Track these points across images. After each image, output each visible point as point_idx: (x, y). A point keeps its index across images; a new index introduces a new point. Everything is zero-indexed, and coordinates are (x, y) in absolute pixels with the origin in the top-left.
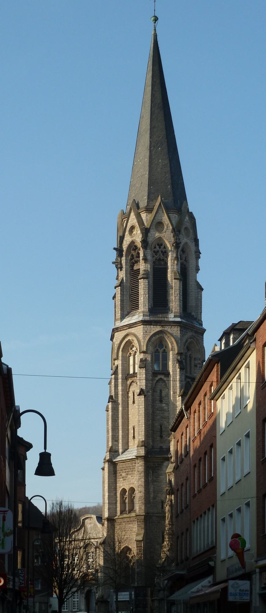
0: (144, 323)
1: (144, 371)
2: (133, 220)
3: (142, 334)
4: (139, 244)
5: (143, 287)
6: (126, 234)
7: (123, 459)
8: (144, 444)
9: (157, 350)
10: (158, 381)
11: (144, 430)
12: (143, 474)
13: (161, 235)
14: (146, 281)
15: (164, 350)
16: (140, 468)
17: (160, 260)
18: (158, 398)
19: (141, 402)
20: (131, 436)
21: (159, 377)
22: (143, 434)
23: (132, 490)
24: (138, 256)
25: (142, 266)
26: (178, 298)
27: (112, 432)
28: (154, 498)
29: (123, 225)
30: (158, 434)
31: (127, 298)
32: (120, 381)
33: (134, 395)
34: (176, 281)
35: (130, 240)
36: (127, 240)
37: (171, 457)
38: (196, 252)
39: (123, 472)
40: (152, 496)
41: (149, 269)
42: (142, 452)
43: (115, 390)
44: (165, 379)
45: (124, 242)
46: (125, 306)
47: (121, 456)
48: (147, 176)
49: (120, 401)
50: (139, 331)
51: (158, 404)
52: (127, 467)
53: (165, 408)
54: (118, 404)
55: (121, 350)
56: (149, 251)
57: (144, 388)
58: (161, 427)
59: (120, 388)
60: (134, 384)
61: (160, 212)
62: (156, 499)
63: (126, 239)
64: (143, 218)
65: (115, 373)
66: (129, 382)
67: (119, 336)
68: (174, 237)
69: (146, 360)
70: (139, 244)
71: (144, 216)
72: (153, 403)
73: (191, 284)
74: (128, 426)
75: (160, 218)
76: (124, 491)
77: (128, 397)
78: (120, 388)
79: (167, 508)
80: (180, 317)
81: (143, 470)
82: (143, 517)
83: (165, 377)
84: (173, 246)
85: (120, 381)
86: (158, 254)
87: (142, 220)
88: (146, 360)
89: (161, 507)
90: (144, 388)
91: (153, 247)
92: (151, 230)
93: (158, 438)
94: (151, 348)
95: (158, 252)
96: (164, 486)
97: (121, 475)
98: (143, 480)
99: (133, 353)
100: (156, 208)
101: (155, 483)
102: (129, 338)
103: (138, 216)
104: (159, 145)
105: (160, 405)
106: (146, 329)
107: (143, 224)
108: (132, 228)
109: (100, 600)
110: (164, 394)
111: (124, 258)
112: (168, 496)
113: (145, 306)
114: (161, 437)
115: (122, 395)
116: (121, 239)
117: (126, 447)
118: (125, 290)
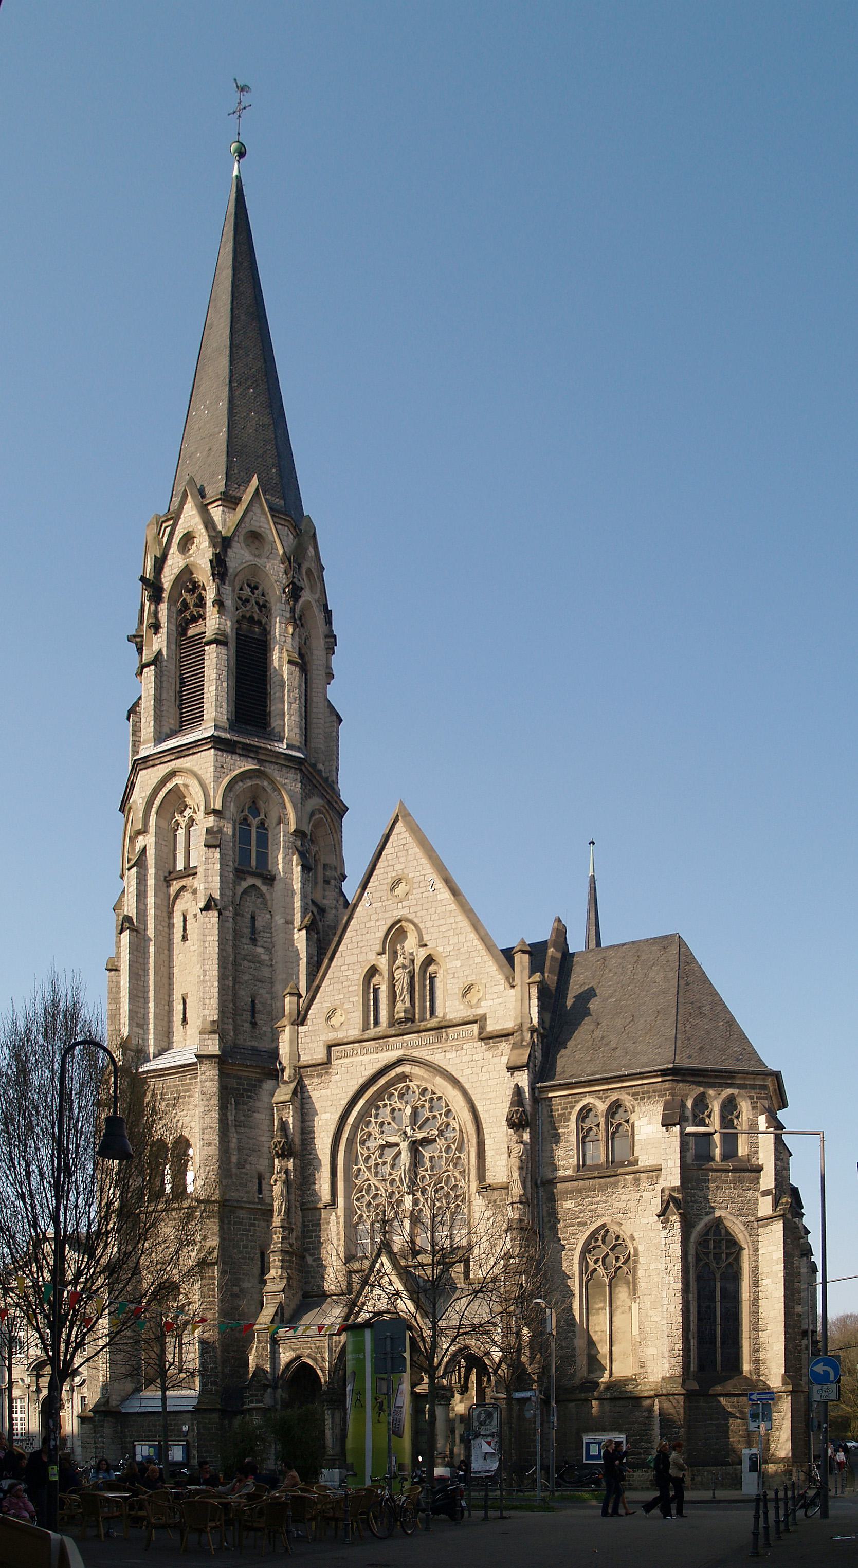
0: (217, 743)
1: (217, 855)
2: (190, 518)
3: (212, 769)
4: (204, 574)
5: (214, 666)
6: (171, 551)
7: (159, 1067)
8: (218, 1028)
9: (245, 819)
10: (245, 892)
11: (216, 995)
12: (215, 1101)
13: (260, 562)
14: (223, 650)
15: (262, 823)
16: (208, 1084)
17: (251, 620)
18: (247, 931)
19: (209, 926)
20: (177, 1017)
21: (251, 881)
22: (216, 1006)
24: (201, 602)
25: (212, 622)
26: (295, 706)
28: (240, 1165)
29: (160, 543)
30: (247, 1016)
31: (169, 695)
32: (151, 882)
33: (185, 920)
34: (293, 668)
35: (182, 564)
36: (174, 564)
37: (283, 1070)
38: (326, 637)
40: (234, 1159)
41: (229, 630)
42: (213, 1048)
44: (264, 889)
45: (166, 570)
46: (164, 713)
47: (152, 1063)
48: (223, 435)
49: (151, 933)
50: (205, 762)
51: (246, 947)
54: (147, 940)
55: (154, 810)
56: (227, 589)
57: (217, 895)
58: (253, 1001)
59: (151, 900)
60: (187, 895)
61: (256, 509)
62: (244, 1167)
63: (169, 562)
64: (215, 518)
65: (140, 862)
66: (173, 889)
67: (148, 779)
68: (286, 573)
69: (220, 831)
70: (204, 574)
71: (216, 512)
72: (235, 938)
73: (318, 709)
77: (171, 926)
78: (151, 900)
79: (277, 1189)
81: (215, 1090)
83: (264, 884)
85: (151, 882)
86: (249, 606)
87: (213, 521)
88: (220, 831)
89: (256, 1187)
90: (217, 895)
91: (238, 587)
92: (235, 544)
93: (247, 1026)
94: (232, 807)
95: (247, 601)
96: (264, 1139)
98: (215, 1114)
99: (183, 822)
100: (247, 497)
101: (242, 1130)
102: (177, 780)
103: (204, 510)
104: (249, 383)
106: (223, 760)
107: (214, 527)
108: (188, 539)
109: (103, 1408)
110: (259, 924)
111: (163, 606)
112: (276, 1161)
113: (218, 707)
114: (254, 1024)
115: (156, 916)
116: (159, 563)
117: (164, 1045)
118: (165, 678)
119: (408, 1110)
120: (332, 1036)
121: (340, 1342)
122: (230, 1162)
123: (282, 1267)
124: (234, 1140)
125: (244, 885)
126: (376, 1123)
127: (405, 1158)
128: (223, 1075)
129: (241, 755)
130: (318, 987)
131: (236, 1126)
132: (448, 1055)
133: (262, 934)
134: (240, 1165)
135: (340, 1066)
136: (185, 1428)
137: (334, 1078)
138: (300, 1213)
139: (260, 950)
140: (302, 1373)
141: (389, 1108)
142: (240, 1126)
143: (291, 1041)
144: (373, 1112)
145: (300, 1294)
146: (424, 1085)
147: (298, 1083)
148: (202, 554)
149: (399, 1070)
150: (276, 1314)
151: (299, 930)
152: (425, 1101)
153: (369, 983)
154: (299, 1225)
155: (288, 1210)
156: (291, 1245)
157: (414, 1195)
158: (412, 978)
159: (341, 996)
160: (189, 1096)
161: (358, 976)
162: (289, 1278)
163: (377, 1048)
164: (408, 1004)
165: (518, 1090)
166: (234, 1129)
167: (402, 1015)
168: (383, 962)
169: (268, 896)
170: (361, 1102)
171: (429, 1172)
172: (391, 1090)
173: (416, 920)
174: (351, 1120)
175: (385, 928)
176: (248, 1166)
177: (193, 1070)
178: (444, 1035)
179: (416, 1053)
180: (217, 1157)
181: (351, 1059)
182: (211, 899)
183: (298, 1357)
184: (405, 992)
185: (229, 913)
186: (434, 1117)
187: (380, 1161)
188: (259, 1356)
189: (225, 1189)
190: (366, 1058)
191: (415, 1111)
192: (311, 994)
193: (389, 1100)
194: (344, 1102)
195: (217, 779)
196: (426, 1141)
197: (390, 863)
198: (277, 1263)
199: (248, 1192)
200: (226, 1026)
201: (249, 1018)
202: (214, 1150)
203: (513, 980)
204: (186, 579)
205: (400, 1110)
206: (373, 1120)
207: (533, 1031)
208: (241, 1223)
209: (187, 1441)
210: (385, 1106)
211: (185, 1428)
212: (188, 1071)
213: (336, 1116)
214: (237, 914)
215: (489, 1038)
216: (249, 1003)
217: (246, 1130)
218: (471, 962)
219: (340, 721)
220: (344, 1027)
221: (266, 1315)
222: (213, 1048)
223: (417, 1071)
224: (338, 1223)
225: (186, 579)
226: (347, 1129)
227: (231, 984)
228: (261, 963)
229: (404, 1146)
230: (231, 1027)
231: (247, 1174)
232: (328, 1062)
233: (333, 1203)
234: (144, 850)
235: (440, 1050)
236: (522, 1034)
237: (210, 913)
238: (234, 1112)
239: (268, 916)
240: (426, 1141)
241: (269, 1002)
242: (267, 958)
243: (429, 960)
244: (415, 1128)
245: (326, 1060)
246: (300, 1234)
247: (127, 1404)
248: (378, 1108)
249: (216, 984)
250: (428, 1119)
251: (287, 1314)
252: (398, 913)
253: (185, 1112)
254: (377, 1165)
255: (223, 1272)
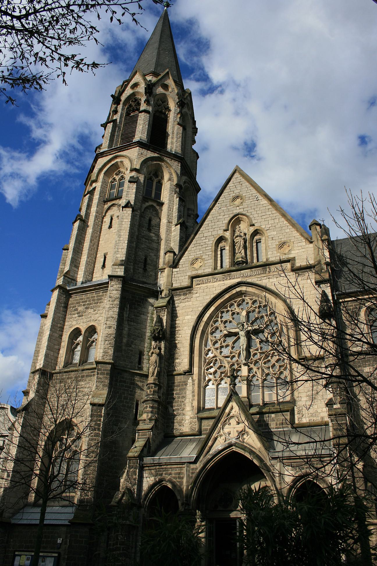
3: (137, 154)
10: (147, 208)
11: (126, 247)
12: (117, 302)
16: (114, 292)
18: (146, 225)
21: (150, 203)
23: (92, 330)
27: (73, 254)
28: (128, 345)
36: (128, 91)
39: (80, 306)
40: (125, 340)
43: (87, 209)
44: (158, 207)
48: (154, 60)
49: (91, 222)
52: (88, 298)
53: (154, 238)
57: (132, 203)
62: (131, 346)
66: (106, 206)
74: (64, 322)
75: (46, 312)
76: (77, 332)
80: (113, 360)
82: (109, 367)
84: (177, 104)
89: (137, 360)
90: (132, 203)
93: (141, 270)
97: (77, 310)
98: (117, 310)
101: (132, 323)
105: (147, 233)
110: (153, 222)
114: (145, 270)
119: (244, 313)
120: (194, 273)
121: (197, 469)
122: (122, 342)
123: (152, 412)
124: (126, 329)
125: (147, 204)
126: (222, 321)
127: (243, 341)
128: (124, 290)
129: (151, 151)
130: (187, 248)
131: (128, 320)
132: (271, 280)
133: (154, 227)
134: (128, 345)
135: (198, 289)
136: (59, 541)
137: (194, 296)
138: (166, 377)
139: (152, 235)
140: (164, 494)
141: (230, 313)
142: (131, 321)
143: (168, 276)
144: (220, 315)
145: (163, 434)
146: (255, 298)
147: (171, 298)
148: (142, 88)
149: (238, 289)
150: (145, 446)
151: (176, 225)
152: (256, 308)
153: (218, 246)
154: (166, 385)
155: (159, 373)
156: (159, 397)
157: (249, 366)
158: (245, 242)
159: (201, 252)
160: (100, 302)
161: (212, 242)
162: (156, 420)
163: (223, 278)
164: (243, 254)
165: (324, 294)
166: (126, 323)
167: (240, 259)
168: (228, 235)
169: (159, 211)
170: (212, 308)
171: (259, 351)
172: (232, 302)
173: (248, 214)
174: (205, 318)
175: (229, 219)
176: (133, 346)
177: (105, 287)
178: (268, 269)
179: (249, 280)
180: (114, 336)
181: (206, 285)
182: (129, 202)
183: (161, 481)
184: (241, 248)
185: (138, 213)
186: (262, 317)
187: (224, 344)
188: (128, 479)
189: (115, 356)
190: (216, 284)
191: (248, 313)
192: (181, 253)
193: (230, 308)
194: (201, 309)
195: (138, 158)
196: (256, 332)
197: (232, 190)
198: (148, 409)
199: (132, 362)
200: (129, 266)
201: (143, 267)
202: (113, 331)
203: (311, 239)
204: (133, 99)
205: (238, 314)
206: (219, 319)
207: (327, 264)
208: (125, 382)
209: (59, 554)
210: (228, 311)
211: (59, 541)
212: (102, 288)
213: (195, 317)
214: (141, 216)
215: (298, 270)
216: (143, 259)
217: (135, 324)
218: (283, 231)
219: (198, 157)
220: (203, 268)
221: (134, 452)
222: (120, 272)
223: (250, 289)
224: (193, 384)
225: (133, 99)
226: (202, 325)
227: (134, 245)
228: (152, 241)
229: (242, 333)
230: (132, 267)
231: (132, 351)
232: (189, 288)
233: (189, 372)
234: (95, 188)
235: (265, 278)
236: (320, 266)
237: (127, 209)
238: (128, 312)
239: (158, 220)
240: (256, 332)
241: (155, 260)
242: (156, 239)
243: (256, 232)
244: (249, 324)
245: (190, 285)
246: (165, 392)
247: (18, 516)
248: (222, 312)
249: (127, 242)
250: (257, 319)
251: (153, 448)
252: (236, 211)
253: (96, 311)
254: (222, 347)
255: (107, 414)
